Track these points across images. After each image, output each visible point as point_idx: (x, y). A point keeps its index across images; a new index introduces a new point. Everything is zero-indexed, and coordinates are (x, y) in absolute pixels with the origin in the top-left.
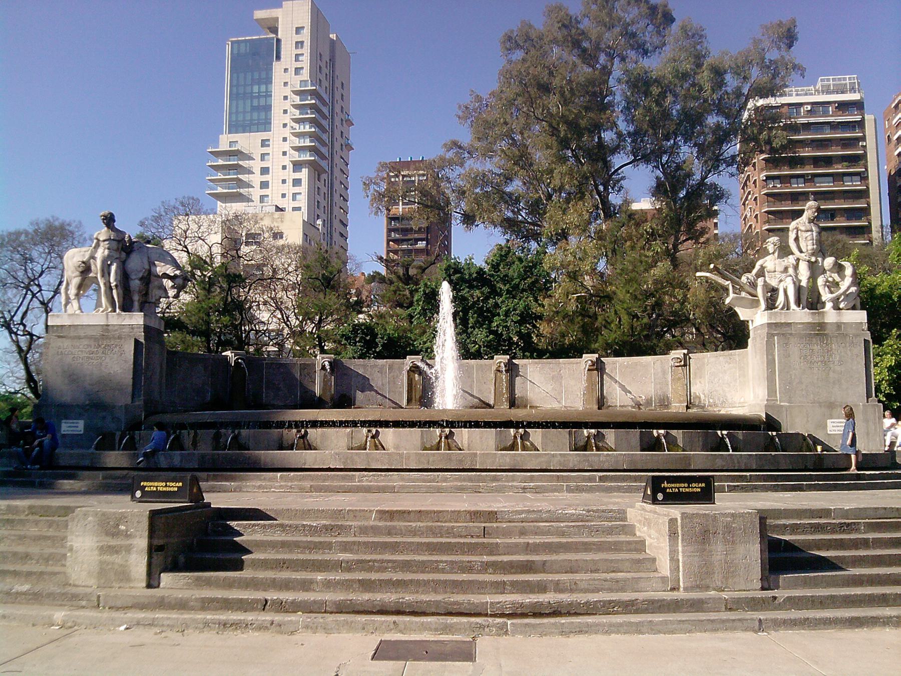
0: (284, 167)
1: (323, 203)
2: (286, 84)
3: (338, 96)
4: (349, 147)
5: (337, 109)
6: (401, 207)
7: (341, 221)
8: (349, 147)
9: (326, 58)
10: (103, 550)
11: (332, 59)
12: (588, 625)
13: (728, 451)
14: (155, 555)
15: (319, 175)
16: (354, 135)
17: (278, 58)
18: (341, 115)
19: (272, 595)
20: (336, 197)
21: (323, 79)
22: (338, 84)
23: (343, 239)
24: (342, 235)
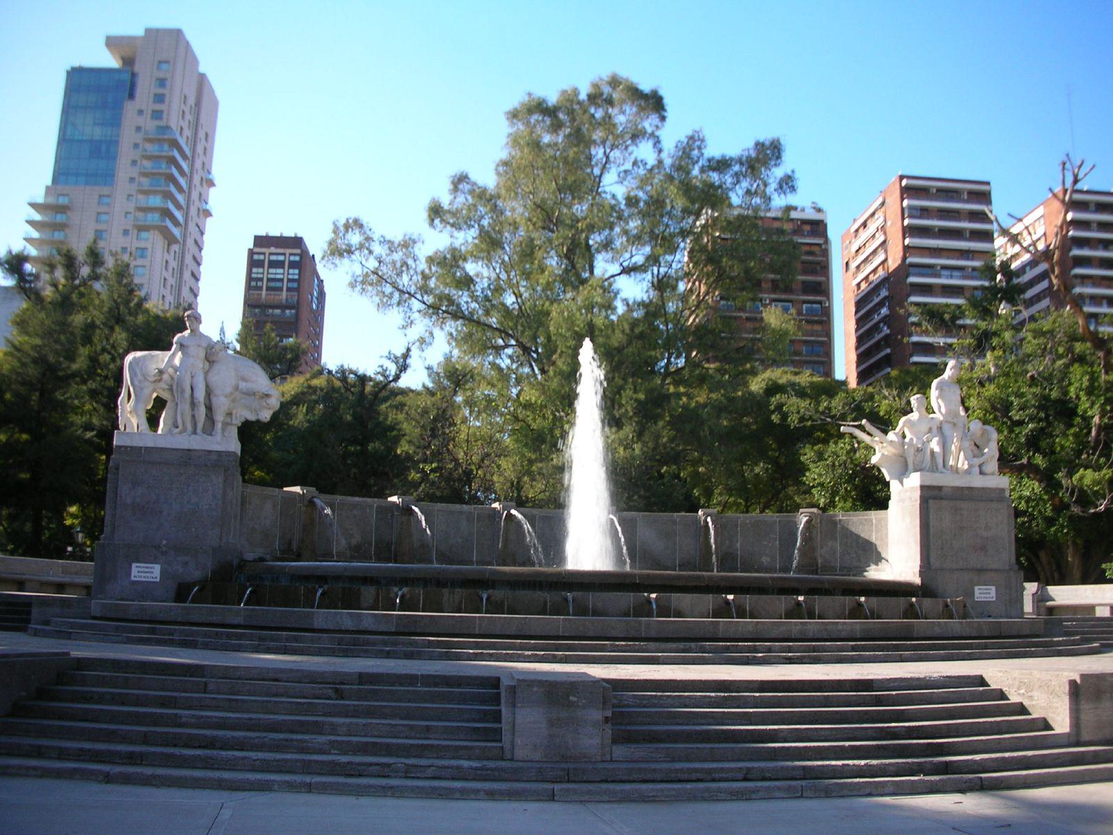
0: (126, 232)
1: (171, 281)
2: (138, 129)
3: (200, 149)
4: (208, 214)
5: (198, 164)
6: (264, 292)
7: (191, 289)
8: (208, 214)
9: (192, 100)
10: (551, 723)
11: (198, 104)
12: (348, 785)
13: (713, 571)
14: (1085, 706)
15: (169, 245)
16: (215, 199)
17: (131, 96)
18: (201, 172)
19: (87, 745)
20: (187, 275)
21: (187, 111)
22: (201, 135)
23: (193, 280)
24: (193, 275)
